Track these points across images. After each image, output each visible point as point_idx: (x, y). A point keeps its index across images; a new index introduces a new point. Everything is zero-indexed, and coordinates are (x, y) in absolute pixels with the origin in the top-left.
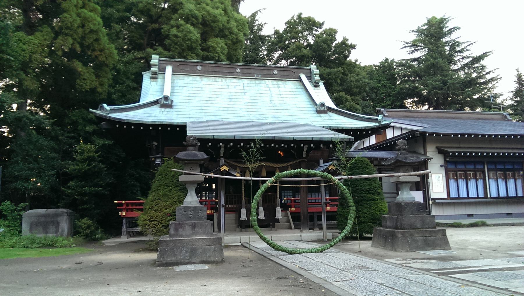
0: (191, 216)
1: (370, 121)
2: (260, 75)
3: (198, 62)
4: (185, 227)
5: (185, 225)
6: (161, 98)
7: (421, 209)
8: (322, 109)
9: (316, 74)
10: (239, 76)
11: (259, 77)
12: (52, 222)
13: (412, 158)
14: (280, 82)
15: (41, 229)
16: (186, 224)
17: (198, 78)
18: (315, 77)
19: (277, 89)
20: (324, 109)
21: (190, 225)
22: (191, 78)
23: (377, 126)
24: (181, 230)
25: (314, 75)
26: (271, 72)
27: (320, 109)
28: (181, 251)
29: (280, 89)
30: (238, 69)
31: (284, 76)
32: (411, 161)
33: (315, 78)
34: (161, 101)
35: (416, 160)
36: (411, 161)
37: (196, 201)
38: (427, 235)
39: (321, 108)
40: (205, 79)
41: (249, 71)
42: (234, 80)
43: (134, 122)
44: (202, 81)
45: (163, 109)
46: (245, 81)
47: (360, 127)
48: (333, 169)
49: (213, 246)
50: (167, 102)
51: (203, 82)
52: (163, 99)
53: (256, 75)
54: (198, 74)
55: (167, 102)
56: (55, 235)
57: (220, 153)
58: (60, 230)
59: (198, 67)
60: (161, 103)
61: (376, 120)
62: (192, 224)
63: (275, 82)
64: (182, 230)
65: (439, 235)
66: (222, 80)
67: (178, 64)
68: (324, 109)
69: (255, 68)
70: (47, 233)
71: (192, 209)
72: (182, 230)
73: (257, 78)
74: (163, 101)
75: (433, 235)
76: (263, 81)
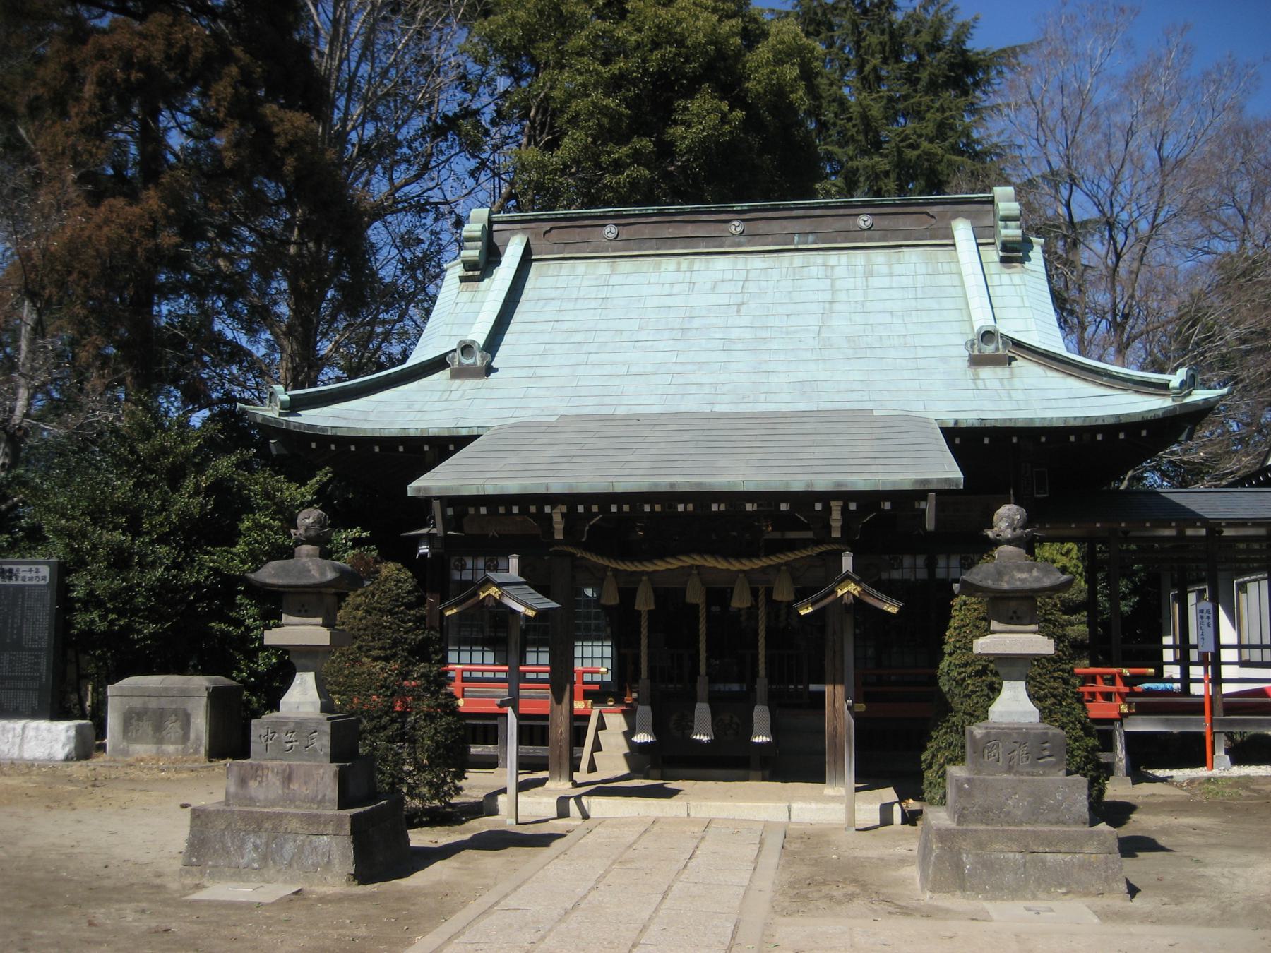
0: (289, 745)
1: (1151, 390)
2: (811, 238)
3: (605, 217)
4: (264, 779)
5: (265, 772)
6: (455, 350)
7: (1046, 753)
8: (989, 349)
9: (1006, 219)
10: (740, 245)
11: (806, 243)
12: (175, 712)
13: (1024, 575)
14: (879, 257)
15: (150, 728)
16: (268, 769)
17: (603, 267)
18: (1006, 227)
19: (860, 282)
20: (997, 349)
21: (277, 773)
22: (581, 266)
23: (1166, 410)
24: (253, 784)
25: (1001, 223)
26: (851, 220)
27: (980, 350)
28: (243, 842)
29: (874, 282)
30: (737, 223)
31: (894, 233)
32: (1018, 583)
33: (1004, 232)
34: (453, 358)
35: (1038, 579)
36: (1018, 583)
37: (313, 703)
38: (1041, 849)
39: (983, 346)
40: (625, 265)
41: (775, 227)
42: (721, 262)
43: (352, 434)
44: (613, 272)
45: (457, 383)
46: (757, 262)
47: (1097, 418)
48: (854, 596)
49: (325, 837)
50: (470, 361)
51: (615, 280)
52: (459, 351)
53: (796, 238)
54: (607, 251)
55: (470, 361)
56: (180, 747)
57: (553, 528)
58: (192, 736)
59: (607, 229)
60: (453, 363)
61: (1163, 388)
62: (284, 771)
63: (859, 257)
64: (257, 784)
65: (1086, 850)
66: (679, 264)
67: (547, 226)
68: (997, 349)
69: (794, 213)
70: (160, 741)
71: (291, 726)
72: (257, 784)
73: (800, 247)
74: (458, 359)
75: (1064, 848)
76: (818, 258)
